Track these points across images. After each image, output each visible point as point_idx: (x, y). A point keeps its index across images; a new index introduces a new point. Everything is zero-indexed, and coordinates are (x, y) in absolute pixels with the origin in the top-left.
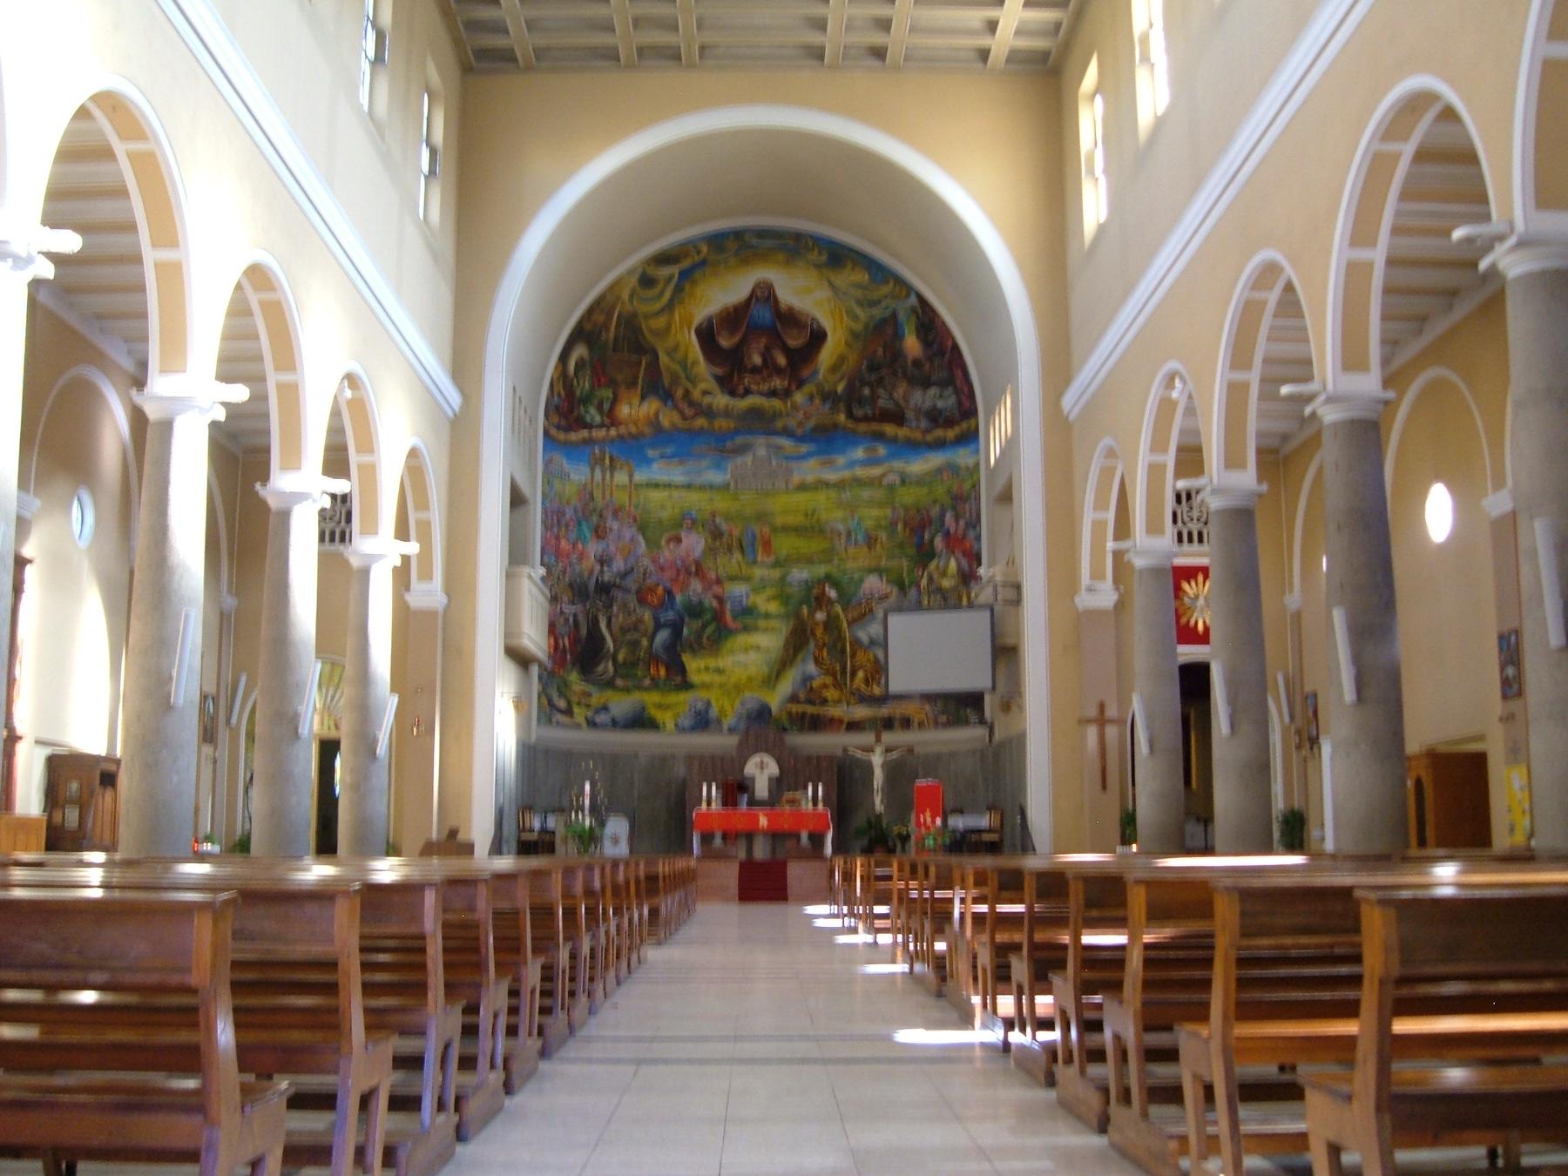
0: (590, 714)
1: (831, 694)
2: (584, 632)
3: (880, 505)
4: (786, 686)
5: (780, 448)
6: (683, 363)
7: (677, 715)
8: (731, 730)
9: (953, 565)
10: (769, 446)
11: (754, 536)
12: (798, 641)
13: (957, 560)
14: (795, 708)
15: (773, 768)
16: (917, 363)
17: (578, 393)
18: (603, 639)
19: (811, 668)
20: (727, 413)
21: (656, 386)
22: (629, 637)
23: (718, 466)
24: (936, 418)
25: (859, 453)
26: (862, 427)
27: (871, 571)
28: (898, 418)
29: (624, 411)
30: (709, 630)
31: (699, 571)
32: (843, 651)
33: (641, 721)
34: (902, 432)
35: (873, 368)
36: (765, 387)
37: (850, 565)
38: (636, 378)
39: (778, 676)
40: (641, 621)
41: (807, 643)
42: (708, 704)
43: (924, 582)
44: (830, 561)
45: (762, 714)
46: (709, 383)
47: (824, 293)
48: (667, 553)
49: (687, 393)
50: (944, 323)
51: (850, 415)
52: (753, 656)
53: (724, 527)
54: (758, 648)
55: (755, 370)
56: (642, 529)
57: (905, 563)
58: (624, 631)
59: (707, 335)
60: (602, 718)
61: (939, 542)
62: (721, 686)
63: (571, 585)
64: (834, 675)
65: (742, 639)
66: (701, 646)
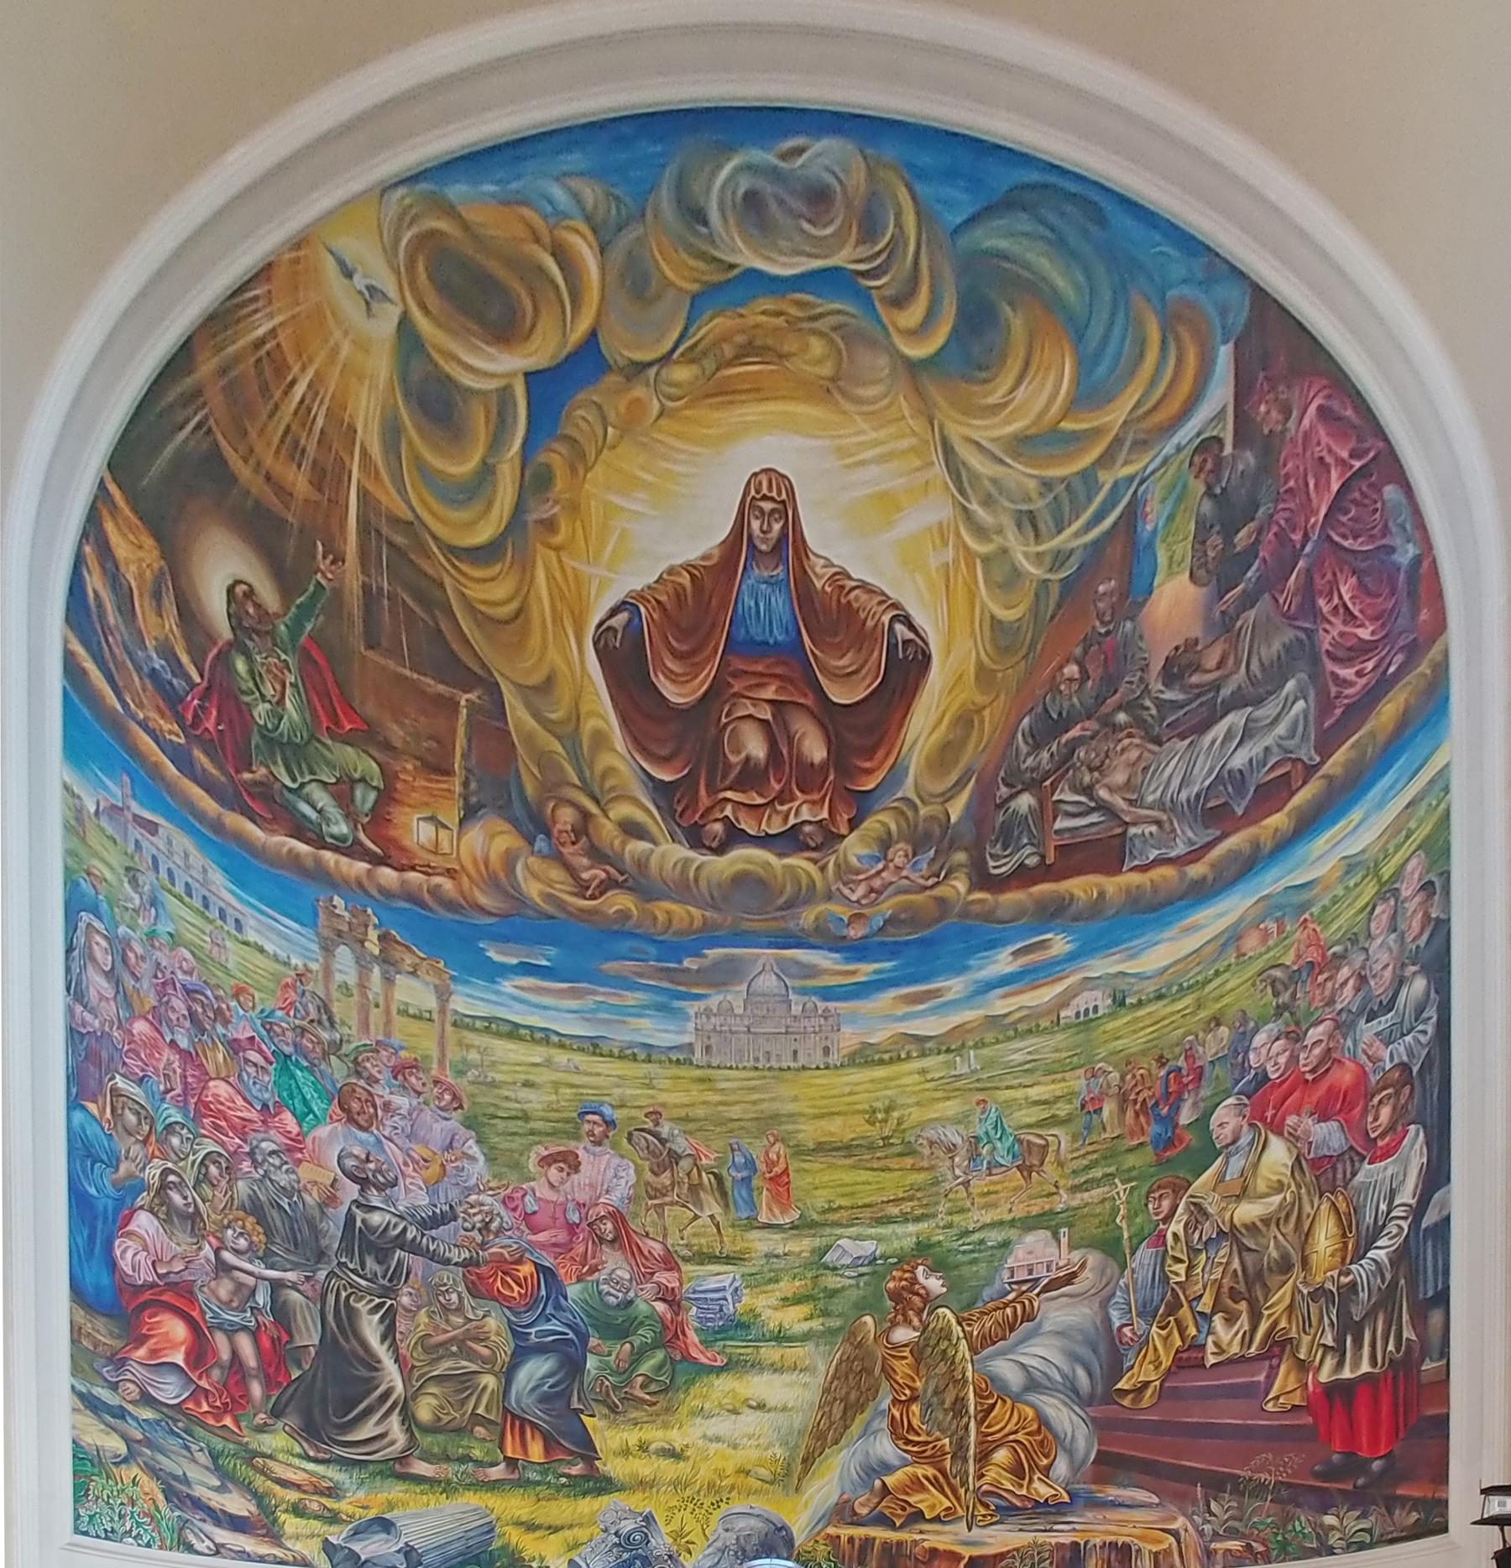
1: (931, 1501)
2: (309, 1336)
4: (828, 1483)
5: (811, 971)
6: (568, 731)
9: (1278, 1154)
10: (785, 969)
11: (750, 1164)
13: (1293, 1139)
18: (373, 1364)
19: (885, 1447)
20: (684, 888)
21: (494, 789)
25: (1003, 962)
30: (646, 1367)
31: (624, 1238)
35: (1048, 728)
38: (445, 744)
39: (808, 1461)
42: (649, 1519)
43: (1177, 1226)
46: (642, 809)
48: (544, 1192)
51: (983, 880)
52: (750, 1421)
53: (681, 1145)
55: (750, 777)
58: (434, 1350)
61: (1226, 1119)
62: (678, 1484)
64: (935, 1460)
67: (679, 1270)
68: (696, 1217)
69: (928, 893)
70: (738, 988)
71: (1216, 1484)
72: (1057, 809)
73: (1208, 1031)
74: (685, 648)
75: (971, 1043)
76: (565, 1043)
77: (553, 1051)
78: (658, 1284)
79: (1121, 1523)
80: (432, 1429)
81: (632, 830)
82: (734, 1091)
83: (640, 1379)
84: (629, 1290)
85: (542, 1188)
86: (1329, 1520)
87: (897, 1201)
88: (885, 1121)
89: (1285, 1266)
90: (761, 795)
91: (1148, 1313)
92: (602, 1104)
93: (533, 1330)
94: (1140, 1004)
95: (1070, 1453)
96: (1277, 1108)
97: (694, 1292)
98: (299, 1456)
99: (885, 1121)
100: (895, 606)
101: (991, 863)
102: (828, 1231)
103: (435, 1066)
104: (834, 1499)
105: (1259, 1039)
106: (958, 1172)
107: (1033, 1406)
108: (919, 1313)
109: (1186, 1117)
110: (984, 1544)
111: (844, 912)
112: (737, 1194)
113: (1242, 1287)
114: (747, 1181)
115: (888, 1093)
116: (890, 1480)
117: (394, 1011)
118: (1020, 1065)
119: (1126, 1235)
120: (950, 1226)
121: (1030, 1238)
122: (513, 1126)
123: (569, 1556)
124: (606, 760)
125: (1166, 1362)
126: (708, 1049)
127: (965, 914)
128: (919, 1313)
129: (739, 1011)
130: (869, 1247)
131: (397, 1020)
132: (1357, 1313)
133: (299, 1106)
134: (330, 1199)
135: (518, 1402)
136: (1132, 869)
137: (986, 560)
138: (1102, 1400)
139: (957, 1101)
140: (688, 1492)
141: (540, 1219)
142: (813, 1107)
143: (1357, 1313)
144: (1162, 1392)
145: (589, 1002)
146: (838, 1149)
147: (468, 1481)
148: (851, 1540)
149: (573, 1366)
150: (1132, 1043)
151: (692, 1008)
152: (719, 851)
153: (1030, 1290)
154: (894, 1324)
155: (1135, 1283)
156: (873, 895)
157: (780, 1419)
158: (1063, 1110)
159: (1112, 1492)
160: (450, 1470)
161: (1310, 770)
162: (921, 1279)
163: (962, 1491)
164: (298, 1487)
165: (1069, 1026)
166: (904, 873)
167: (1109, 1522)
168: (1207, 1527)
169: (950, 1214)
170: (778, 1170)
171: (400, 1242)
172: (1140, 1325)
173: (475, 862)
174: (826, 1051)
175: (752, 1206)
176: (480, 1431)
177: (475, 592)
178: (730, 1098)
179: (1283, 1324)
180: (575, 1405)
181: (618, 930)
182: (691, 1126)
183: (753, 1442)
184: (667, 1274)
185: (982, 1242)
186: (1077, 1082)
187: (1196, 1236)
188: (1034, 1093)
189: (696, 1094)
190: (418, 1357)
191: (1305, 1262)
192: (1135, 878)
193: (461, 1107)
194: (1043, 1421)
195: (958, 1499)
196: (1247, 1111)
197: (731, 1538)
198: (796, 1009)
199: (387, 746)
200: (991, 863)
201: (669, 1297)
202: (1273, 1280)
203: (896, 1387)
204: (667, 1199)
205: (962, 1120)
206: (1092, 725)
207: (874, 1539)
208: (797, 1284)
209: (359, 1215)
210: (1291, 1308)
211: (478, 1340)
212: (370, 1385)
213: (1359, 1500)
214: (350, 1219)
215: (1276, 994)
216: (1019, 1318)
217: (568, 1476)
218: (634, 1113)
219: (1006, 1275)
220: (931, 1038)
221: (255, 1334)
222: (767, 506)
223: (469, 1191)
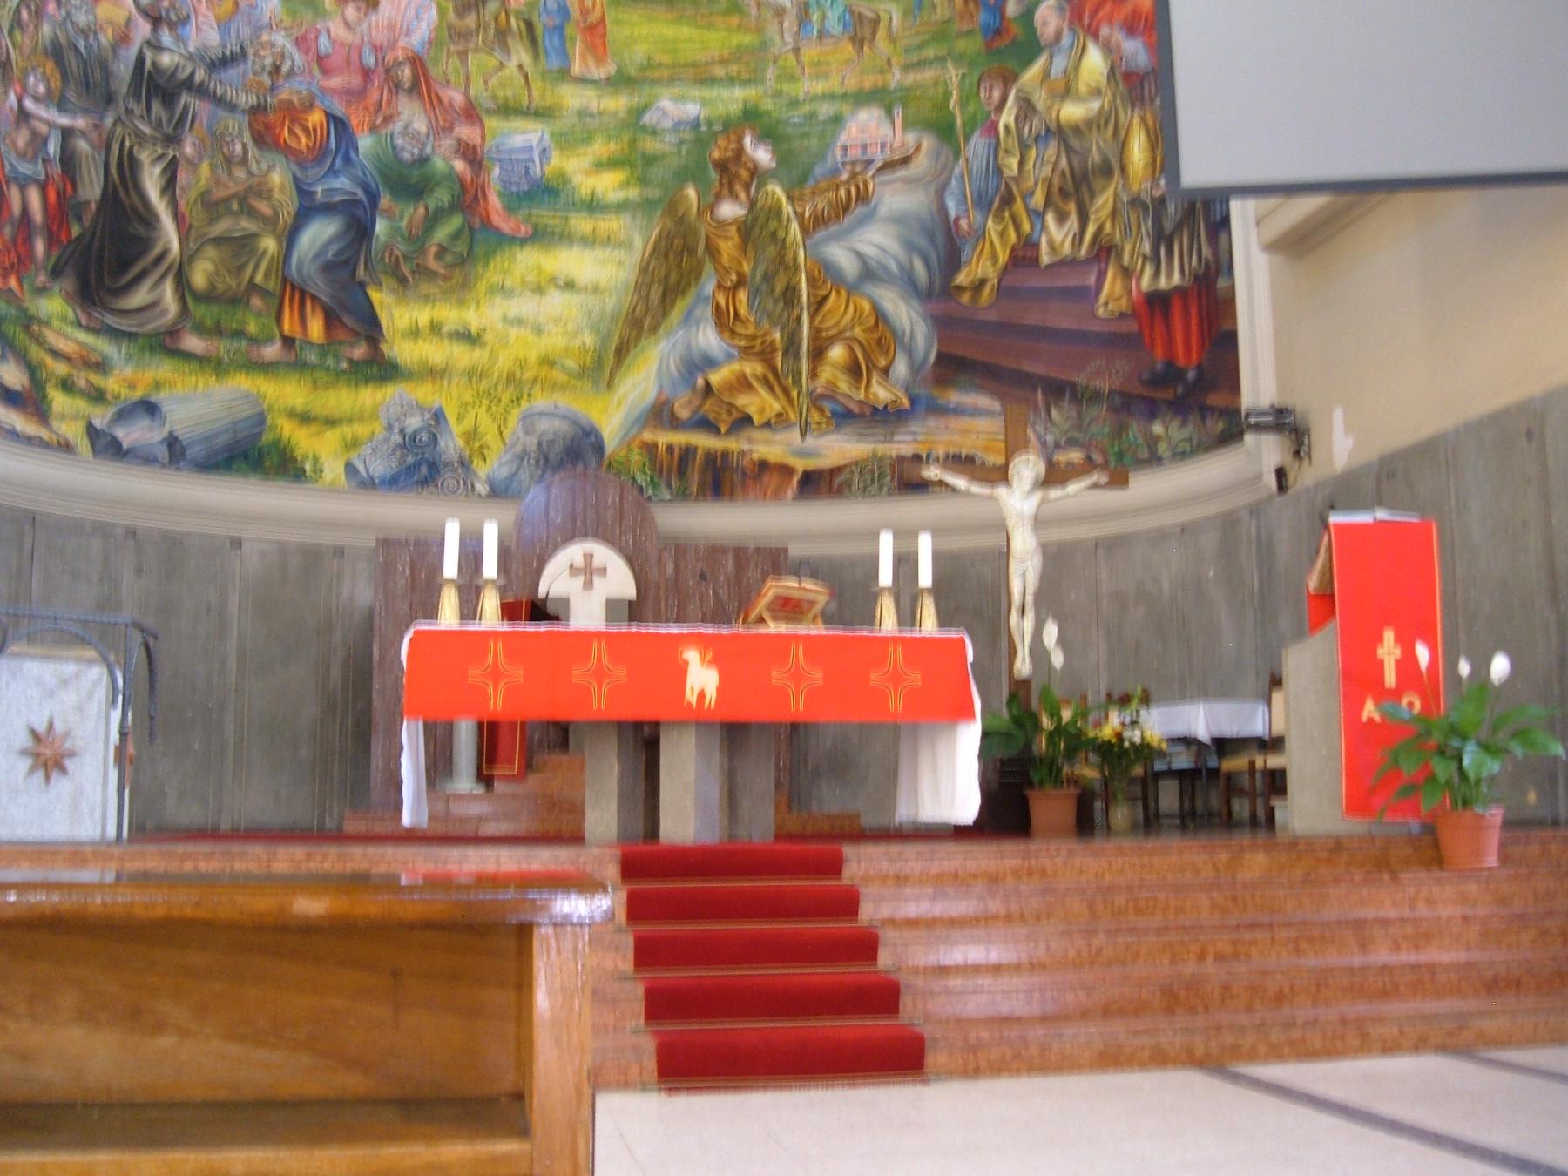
1: (760, 403)
2: (92, 189)
4: (643, 381)
7: (352, 444)
9: (1094, 62)
12: (672, 270)
13: (1108, 48)
14: (664, 438)
15: (620, 581)
18: (149, 219)
19: (708, 338)
22: (222, 227)
27: (862, 98)
30: (442, 233)
31: (421, 84)
32: (790, 294)
33: (250, 453)
37: (806, 86)
39: (622, 352)
40: (262, 191)
41: (697, 273)
42: (439, 416)
43: (1007, 117)
44: (754, 79)
45: (577, 451)
48: (338, 30)
52: (556, 301)
54: (569, 285)
57: (953, 74)
58: (213, 207)
60: (133, 434)
62: (474, 374)
63: (46, 52)
64: (766, 355)
65: (527, 261)
66: (422, 271)
67: (483, 127)
71: (1057, 390)
79: (965, 432)
80: (209, 297)
86: (1158, 428)
87: (723, 61)
89: (1106, 170)
91: (983, 203)
95: (910, 352)
96: (1092, 17)
98: (72, 324)
104: (651, 396)
108: (747, 187)
112: (548, 42)
113: (1070, 186)
116: (715, 378)
119: (959, 122)
125: (1003, 257)
128: (747, 187)
130: (692, 110)
132: (1168, 226)
134: (123, 39)
135: (299, 268)
138: (939, 292)
140: (484, 385)
143: (1168, 226)
144: (999, 289)
148: (670, 448)
149: (359, 230)
154: (718, 197)
155: (970, 172)
157: (593, 302)
159: (955, 397)
160: (223, 347)
163: (795, 394)
164: (68, 359)
171: (188, 84)
172: (976, 216)
175: (565, 55)
176: (256, 302)
179: (1108, 228)
187: (1027, 129)
190: (196, 215)
191: (1123, 169)
194: (880, 316)
195: (790, 401)
197: (532, 442)
202: (1097, 183)
203: (722, 271)
207: (696, 449)
210: (1114, 214)
212: (144, 244)
213: (1179, 408)
214: (140, 60)
216: (851, 203)
219: (839, 153)
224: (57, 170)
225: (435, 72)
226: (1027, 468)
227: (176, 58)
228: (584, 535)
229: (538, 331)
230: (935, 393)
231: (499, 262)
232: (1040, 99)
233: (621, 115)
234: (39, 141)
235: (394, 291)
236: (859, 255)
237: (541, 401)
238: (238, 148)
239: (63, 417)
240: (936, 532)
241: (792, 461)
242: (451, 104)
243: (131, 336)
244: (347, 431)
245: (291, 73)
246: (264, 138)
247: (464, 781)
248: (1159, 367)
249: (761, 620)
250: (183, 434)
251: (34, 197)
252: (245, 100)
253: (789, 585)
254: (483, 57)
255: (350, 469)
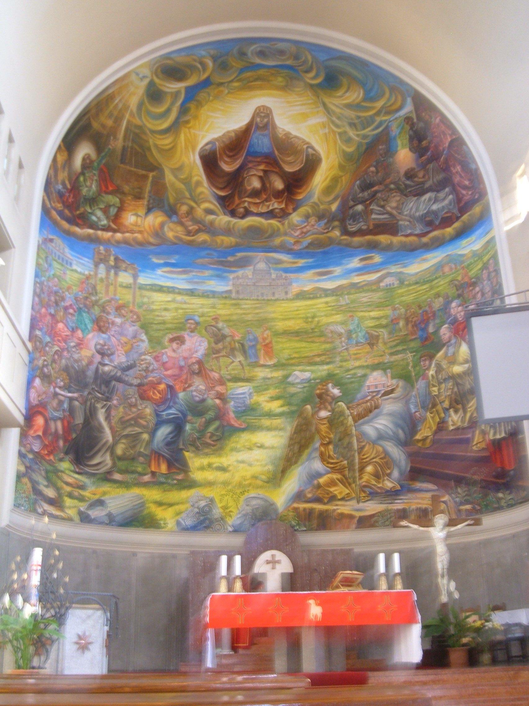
0: (83, 507)
1: (339, 490)
2: (79, 420)
3: (379, 306)
4: (292, 483)
5: (279, 262)
6: (187, 182)
8: (236, 531)
10: (268, 261)
14: (302, 506)
15: (285, 566)
16: (410, 175)
17: (84, 191)
18: (100, 429)
19: (318, 465)
20: (228, 231)
21: (159, 202)
23: (219, 277)
24: (431, 222)
25: (355, 263)
26: (357, 240)
27: (375, 367)
28: (390, 228)
29: (130, 219)
30: (211, 429)
32: (349, 446)
33: (138, 519)
34: (396, 240)
35: (366, 186)
36: (263, 209)
37: (351, 364)
40: (140, 416)
42: (212, 500)
43: (432, 372)
45: (264, 515)
46: (213, 205)
47: (318, 119)
48: (171, 354)
49: (190, 211)
50: (445, 121)
51: (345, 232)
52: (257, 454)
53: (227, 331)
54: (261, 447)
56: (145, 327)
58: (124, 423)
59: (210, 161)
60: (94, 513)
61: (445, 332)
62: (225, 483)
64: (340, 471)
65: (245, 438)
68: (233, 362)
69: (325, 235)
70: (250, 268)
72: (372, 212)
73: (435, 298)
74: (231, 154)
75: (346, 292)
76: (180, 292)
77: (176, 295)
78: (217, 391)
81: (209, 212)
82: (248, 309)
83: (209, 434)
84: (204, 394)
85: (169, 353)
87: (319, 355)
88: (312, 322)
90: (259, 199)
92: (194, 315)
93: (164, 413)
94: (410, 285)
95: (399, 467)
97: (233, 395)
99: (312, 322)
100: (308, 143)
101: (349, 227)
102: (290, 368)
103: (131, 305)
105: (454, 304)
106: (344, 344)
107: (381, 446)
109: (431, 329)
110: (367, 510)
111: (292, 241)
112: (250, 352)
114: (254, 346)
115: (313, 310)
117: (118, 285)
118: (366, 302)
119: (413, 374)
120: (341, 367)
121: (375, 374)
122: (159, 327)
123: (177, 518)
124: (200, 190)
125: (434, 428)
126: (238, 292)
127: (339, 244)
129: (250, 277)
130: (307, 375)
131: (119, 289)
133: (83, 327)
134: (90, 363)
136: (402, 235)
137: (340, 134)
139: (341, 315)
140: (230, 487)
141: (169, 365)
142: (282, 315)
145: (191, 275)
146: (292, 333)
147: (136, 482)
149: (178, 426)
150: (409, 299)
151: (231, 276)
152: (243, 217)
153: (377, 395)
154: (320, 409)
156: (303, 234)
158: (384, 322)
159: (418, 485)
160: (128, 477)
161: (458, 218)
162: (331, 389)
165: (384, 290)
166: (315, 227)
167: (419, 498)
168: (458, 499)
169: (341, 361)
170: (267, 341)
173: (150, 228)
174: (286, 293)
176: (141, 459)
177: (159, 142)
178: (248, 311)
180: (181, 446)
181: (203, 246)
182: (231, 324)
183: (258, 463)
184: (221, 387)
185: (355, 374)
186: (388, 311)
188: (372, 314)
189: (232, 310)
192: (403, 239)
193: (140, 321)
194: (386, 454)
196: (453, 330)
198: (274, 276)
199: (123, 193)
200: (349, 227)
201: (220, 396)
203: (322, 438)
204: (221, 354)
205: (343, 323)
206: (382, 187)
208: (277, 391)
209: (100, 366)
211: (142, 418)
214: (97, 369)
215: (457, 290)
216: (370, 411)
217: (178, 480)
218: (208, 319)
219: (366, 388)
220: (330, 290)
221: (62, 420)
222: (263, 115)
223: (142, 354)
224: (67, 413)
225: (207, 366)
226: (440, 520)
227: (111, 368)
228: (272, 549)
229: (250, 465)
230: (410, 483)
231: (234, 438)
232: (444, 364)
233: (280, 378)
234: (61, 403)
235: (193, 452)
236: (377, 429)
237: (252, 493)
238: (134, 400)
239: (70, 508)
240: (400, 552)
241: (354, 513)
242: (214, 377)
243: (94, 475)
244: (177, 508)
245: (153, 370)
246: (143, 397)
247: (227, 651)
248: (499, 469)
249: (337, 587)
250: (114, 512)
251: (59, 424)
252: (136, 382)
253: (348, 573)
254: (226, 359)
255: (178, 523)
